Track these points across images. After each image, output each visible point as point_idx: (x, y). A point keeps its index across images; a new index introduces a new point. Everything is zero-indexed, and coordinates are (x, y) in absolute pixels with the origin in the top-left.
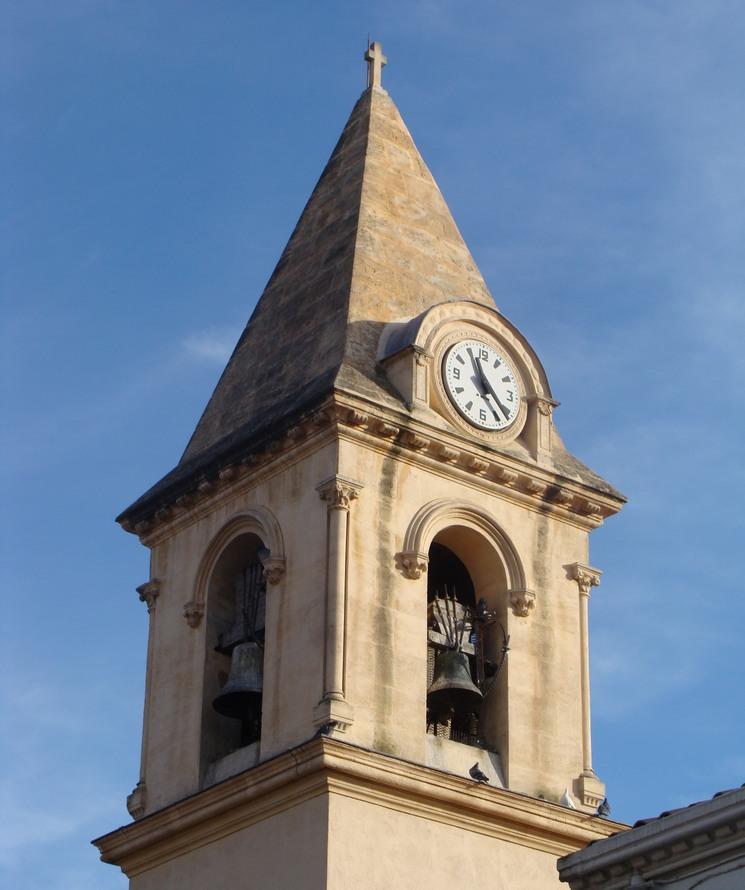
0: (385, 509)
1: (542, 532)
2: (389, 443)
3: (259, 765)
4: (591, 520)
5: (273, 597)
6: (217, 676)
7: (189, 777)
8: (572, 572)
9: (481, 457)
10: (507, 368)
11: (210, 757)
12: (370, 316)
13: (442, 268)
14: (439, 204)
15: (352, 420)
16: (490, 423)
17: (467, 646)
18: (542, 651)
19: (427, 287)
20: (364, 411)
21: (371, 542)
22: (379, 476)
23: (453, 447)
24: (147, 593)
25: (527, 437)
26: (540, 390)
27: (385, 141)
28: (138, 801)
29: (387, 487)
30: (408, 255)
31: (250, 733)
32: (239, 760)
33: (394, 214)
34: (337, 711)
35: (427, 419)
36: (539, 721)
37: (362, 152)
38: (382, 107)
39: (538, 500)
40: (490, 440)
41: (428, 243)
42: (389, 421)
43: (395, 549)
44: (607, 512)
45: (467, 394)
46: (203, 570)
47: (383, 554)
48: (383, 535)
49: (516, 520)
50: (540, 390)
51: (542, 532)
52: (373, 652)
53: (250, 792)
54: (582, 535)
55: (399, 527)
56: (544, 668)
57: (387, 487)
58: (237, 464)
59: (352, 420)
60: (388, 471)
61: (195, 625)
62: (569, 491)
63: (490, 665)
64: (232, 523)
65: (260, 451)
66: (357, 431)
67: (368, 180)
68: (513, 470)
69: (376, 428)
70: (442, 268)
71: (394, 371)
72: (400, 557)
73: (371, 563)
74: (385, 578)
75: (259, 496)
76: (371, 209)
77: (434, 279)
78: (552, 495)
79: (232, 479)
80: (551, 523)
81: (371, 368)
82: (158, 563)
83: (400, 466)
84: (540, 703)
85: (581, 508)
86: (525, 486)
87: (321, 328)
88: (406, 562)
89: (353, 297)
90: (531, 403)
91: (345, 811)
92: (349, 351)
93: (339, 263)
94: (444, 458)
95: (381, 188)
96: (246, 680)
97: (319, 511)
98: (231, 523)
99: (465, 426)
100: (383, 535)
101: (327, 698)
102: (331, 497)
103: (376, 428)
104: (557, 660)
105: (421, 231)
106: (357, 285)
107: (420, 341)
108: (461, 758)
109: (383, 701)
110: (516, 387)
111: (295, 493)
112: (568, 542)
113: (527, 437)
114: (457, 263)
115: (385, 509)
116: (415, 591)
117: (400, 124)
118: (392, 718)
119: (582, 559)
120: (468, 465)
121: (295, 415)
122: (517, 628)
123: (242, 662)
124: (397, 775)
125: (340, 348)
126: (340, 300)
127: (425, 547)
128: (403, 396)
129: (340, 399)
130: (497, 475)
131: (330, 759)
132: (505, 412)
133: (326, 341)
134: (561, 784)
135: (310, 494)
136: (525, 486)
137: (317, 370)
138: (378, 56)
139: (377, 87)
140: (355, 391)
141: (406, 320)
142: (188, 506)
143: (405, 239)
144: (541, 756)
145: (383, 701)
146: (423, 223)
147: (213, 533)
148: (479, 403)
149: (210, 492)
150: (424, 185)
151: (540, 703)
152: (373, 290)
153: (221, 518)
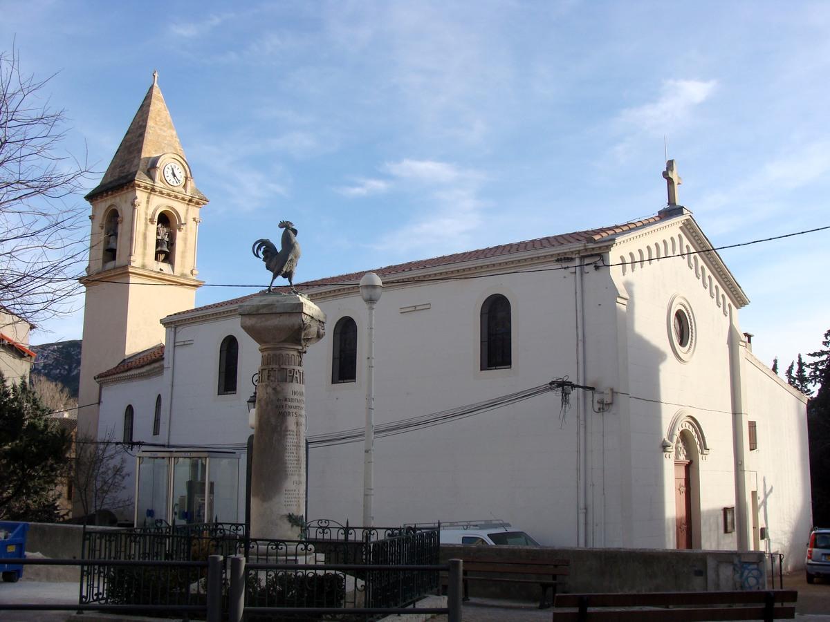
0: (147, 207)
1: (187, 210)
2: (149, 191)
3: (115, 268)
4: (200, 206)
5: (120, 226)
6: (107, 242)
7: (98, 265)
8: (194, 219)
9: (172, 193)
10: (181, 169)
11: (105, 262)
12: (147, 156)
13: (168, 138)
14: (169, 119)
15: (139, 186)
16: (175, 184)
17: (166, 239)
18: (185, 240)
19: (163, 145)
20: (143, 185)
21: (143, 216)
22: (146, 199)
23: (165, 191)
24: (91, 218)
25: (185, 186)
26: (189, 175)
27: (156, 102)
28: (88, 269)
29: (148, 202)
30: (159, 135)
31: (114, 258)
32: (110, 265)
33: (156, 124)
34: (132, 258)
35: (159, 185)
36: (183, 257)
37: (149, 105)
38: (157, 92)
39: (187, 202)
40: (175, 189)
41: (164, 131)
42: (149, 186)
43: (149, 217)
44: (204, 204)
45: (170, 178)
46: (104, 215)
47: (146, 218)
48: (146, 214)
49: (180, 208)
50: (189, 175)
51: (187, 210)
52: (142, 243)
53: (112, 274)
54: (199, 209)
55: (150, 212)
56: (185, 244)
57: (148, 202)
58: (112, 191)
59: (139, 186)
60: (148, 198)
61: (102, 229)
62: (194, 200)
63: (171, 244)
64: (112, 205)
65: (118, 189)
66: (141, 189)
67: (151, 114)
68: (180, 196)
69: (146, 188)
70: (168, 138)
71: (152, 171)
72: (150, 219)
73: (143, 221)
74: (146, 225)
75: (118, 199)
76: (150, 123)
77: (166, 142)
78: (190, 201)
79: (112, 194)
80: (190, 207)
81: (146, 171)
82: (94, 210)
83: (152, 196)
84: (184, 252)
85: (198, 203)
86: (183, 199)
87: (135, 157)
88: (152, 221)
89: (143, 150)
90: (186, 178)
91: (132, 279)
92: (141, 167)
93: (141, 139)
94: (163, 194)
95: (153, 116)
96: (112, 246)
97: (131, 208)
98: (109, 207)
99: (169, 186)
100: (146, 214)
101: (130, 255)
102: (134, 206)
103: (146, 188)
104: (188, 242)
105: (163, 128)
106: (144, 146)
107: (158, 165)
108: (166, 267)
109: (144, 255)
110: (183, 174)
111: (126, 202)
112: (194, 211)
113: (185, 186)
114: (172, 136)
115: (147, 207)
116: (153, 228)
117: (161, 95)
118: (146, 259)
119: (197, 217)
120: (169, 195)
121: (126, 183)
122: (179, 235)
123: (15, 478)
124: (146, 273)
125: (138, 165)
126: (140, 151)
127: (156, 217)
128: (152, 179)
129: (136, 182)
130: (176, 197)
131: (130, 270)
132: (179, 181)
133: (136, 162)
134: (188, 272)
135: (129, 204)
136: (183, 199)
137: (133, 170)
138: (156, 75)
139: (156, 84)
140: (141, 179)
141: (156, 155)
142: (101, 198)
143: (159, 131)
144: (183, 265)
145: (144, 255)
146: (164, 125)
147: (107, 206)
148: (173, 179)
149: (107, 196)
150: (166, 114)
151: (184, 252)
152: (149, 148)
153: (109, 203)
